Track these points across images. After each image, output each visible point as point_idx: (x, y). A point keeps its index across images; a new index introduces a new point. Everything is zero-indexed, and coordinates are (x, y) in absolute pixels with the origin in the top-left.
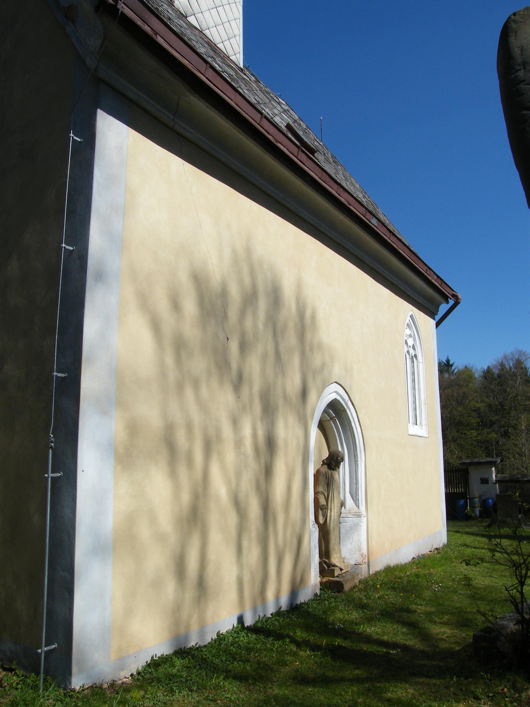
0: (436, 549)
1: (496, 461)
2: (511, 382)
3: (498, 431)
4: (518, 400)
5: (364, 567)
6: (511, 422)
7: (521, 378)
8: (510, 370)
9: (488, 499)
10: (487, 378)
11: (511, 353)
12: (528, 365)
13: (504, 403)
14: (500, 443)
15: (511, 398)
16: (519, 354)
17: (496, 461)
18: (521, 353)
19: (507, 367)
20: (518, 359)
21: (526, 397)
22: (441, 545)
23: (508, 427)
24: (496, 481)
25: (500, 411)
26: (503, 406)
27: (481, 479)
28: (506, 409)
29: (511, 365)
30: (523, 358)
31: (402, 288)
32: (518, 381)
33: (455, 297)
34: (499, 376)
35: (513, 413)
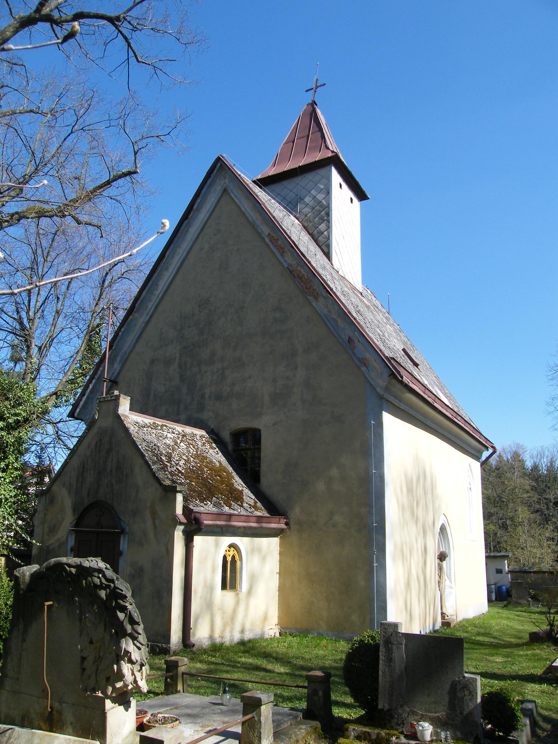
0: (483, 614)
1: (509, 556)
2: (509, 475)
3: (496, 522)
4: (515, 492)
5: (455, 617)
6: (509, 514)
7: (519, 471)
8: (508, 460)
9: (502, 586)
10: (486, 470)
11: (509, 446)
12: (526, 458)
13: (502, 495)
14: (498, 534)
15: (509, 490)
16: (517, 447)
17: (509, 556)
18: (518, 445)
19: (505, 459)
20: (516, 452)
21: (523, 490)
22: (485, 612)
23: (506, 519)
24: (508, 571)
25: (498, 503)
26: (500, 497)
27: (496, 569)
28: (503, 502)
29: (509, 457)
30: (521, 452)
31: (466, 448)
32: (516, 474)
33: (493, 447)
34: (497, 469)
35: (511, 505)
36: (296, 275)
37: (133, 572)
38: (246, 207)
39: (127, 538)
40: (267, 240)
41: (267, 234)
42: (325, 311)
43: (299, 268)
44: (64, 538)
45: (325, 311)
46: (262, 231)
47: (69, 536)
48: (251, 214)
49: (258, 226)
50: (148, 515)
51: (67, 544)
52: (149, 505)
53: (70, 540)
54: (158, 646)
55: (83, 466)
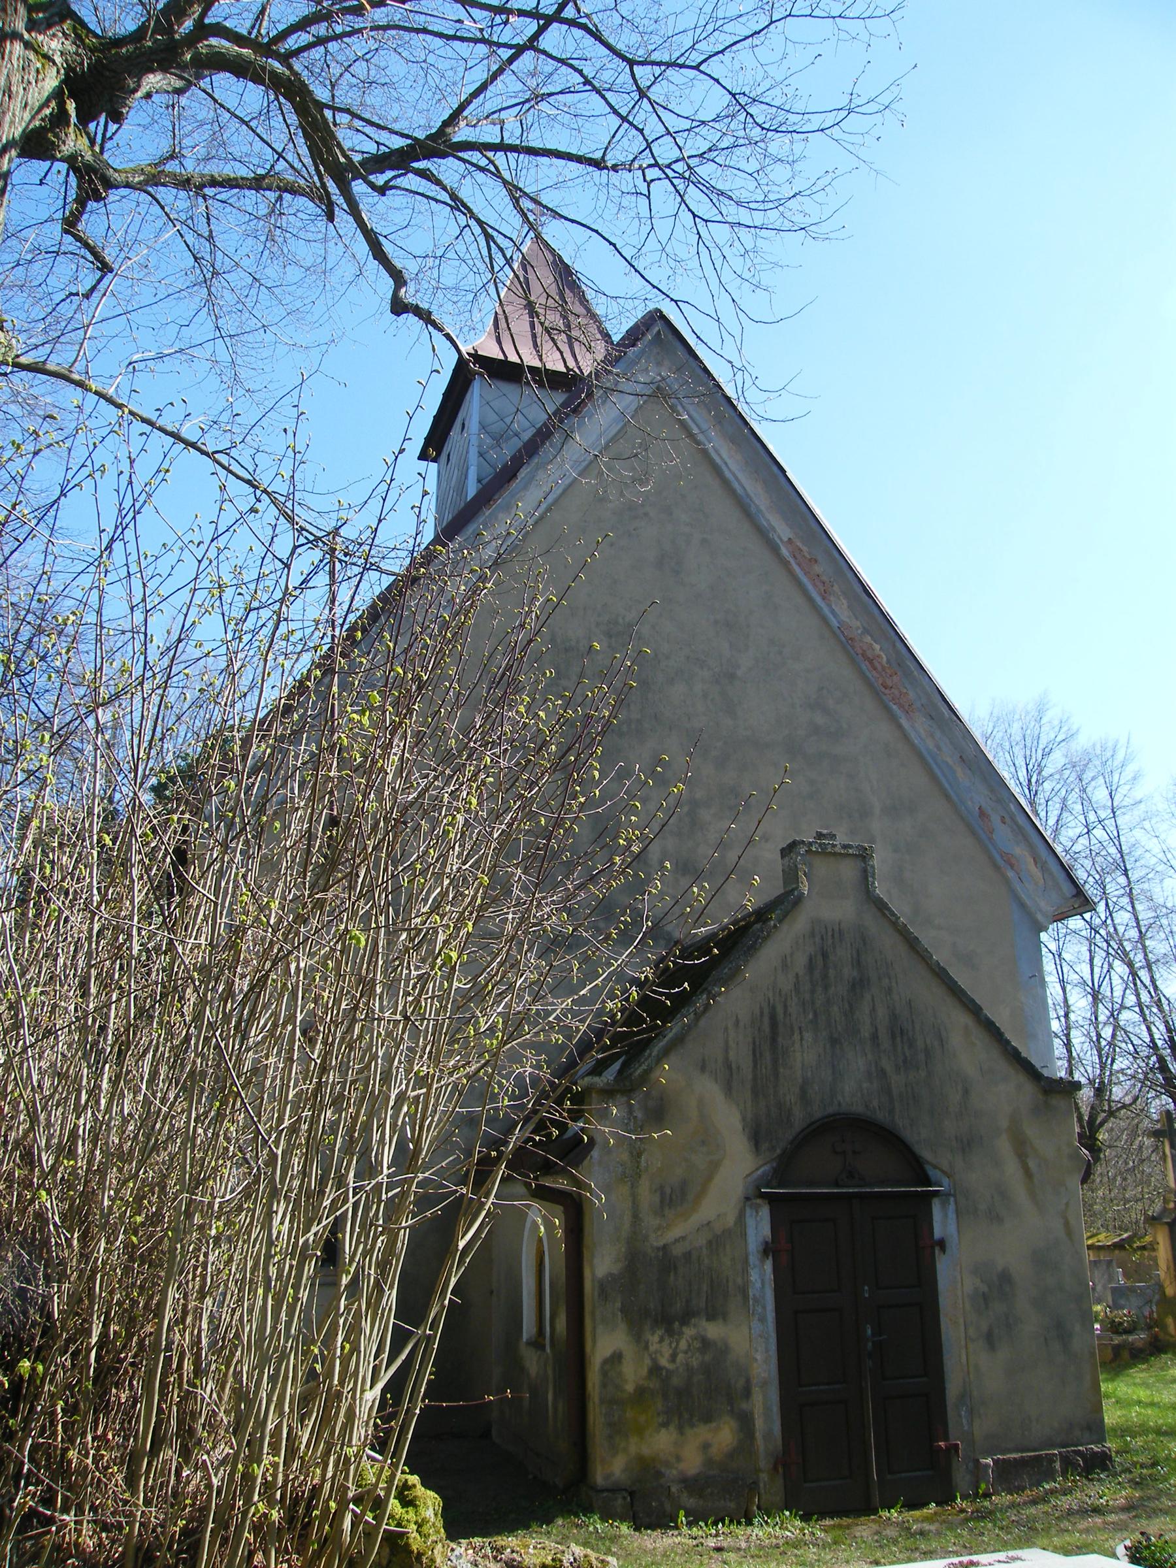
36: (860, 651)
37: (985, 1289)
38: (725, 456)
39: (952, 1207)
40: (784, 551)
41: (785, 539)
42: (930, 744)
43: (868, 639)
44: (731, 1220)
45: (930, 744)
46: (770, 524)
47: (748, 1211)
48: (740, 475)
49: (759, 511)
50: (1004, 1146)
51: (744, 1235)
52: (1004, 1123)
53: (750, 1222)
54: (1078, 1453)
55: (773, 1018)
